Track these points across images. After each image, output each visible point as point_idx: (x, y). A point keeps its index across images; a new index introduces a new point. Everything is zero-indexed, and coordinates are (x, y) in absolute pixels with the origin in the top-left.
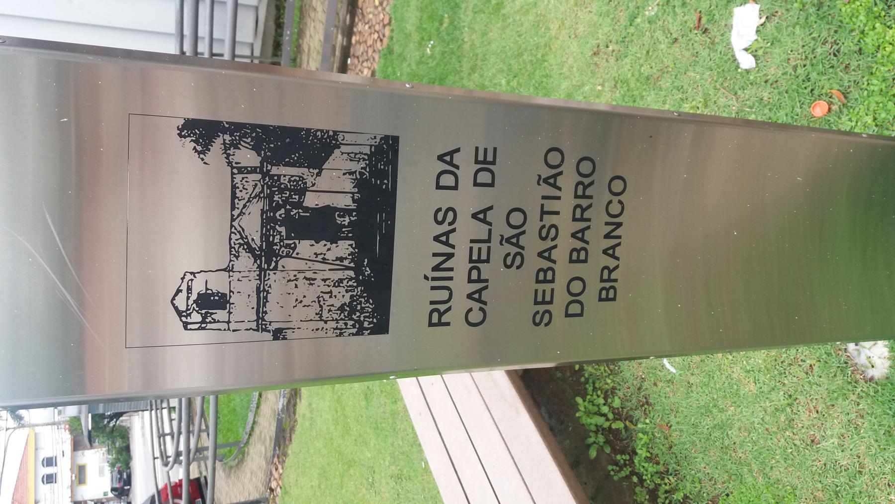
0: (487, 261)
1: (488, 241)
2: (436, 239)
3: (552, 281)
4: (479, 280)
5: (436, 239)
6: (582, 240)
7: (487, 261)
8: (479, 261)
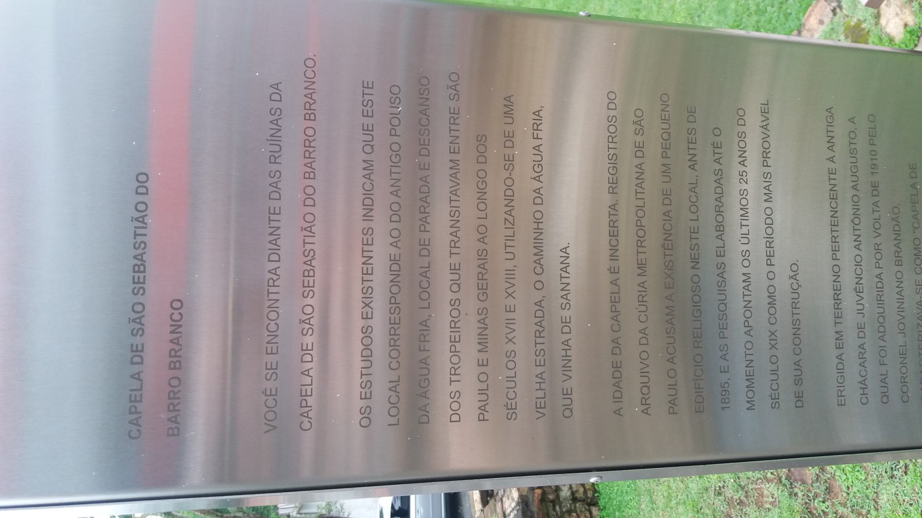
0: (141, 401)
1: (141, 389)
2: (135, 257)
3: (144, 272)
4: (136, 412)
5: (135, 257)
6: (141, 260)
7: (141, 401)
8: (136, 401)
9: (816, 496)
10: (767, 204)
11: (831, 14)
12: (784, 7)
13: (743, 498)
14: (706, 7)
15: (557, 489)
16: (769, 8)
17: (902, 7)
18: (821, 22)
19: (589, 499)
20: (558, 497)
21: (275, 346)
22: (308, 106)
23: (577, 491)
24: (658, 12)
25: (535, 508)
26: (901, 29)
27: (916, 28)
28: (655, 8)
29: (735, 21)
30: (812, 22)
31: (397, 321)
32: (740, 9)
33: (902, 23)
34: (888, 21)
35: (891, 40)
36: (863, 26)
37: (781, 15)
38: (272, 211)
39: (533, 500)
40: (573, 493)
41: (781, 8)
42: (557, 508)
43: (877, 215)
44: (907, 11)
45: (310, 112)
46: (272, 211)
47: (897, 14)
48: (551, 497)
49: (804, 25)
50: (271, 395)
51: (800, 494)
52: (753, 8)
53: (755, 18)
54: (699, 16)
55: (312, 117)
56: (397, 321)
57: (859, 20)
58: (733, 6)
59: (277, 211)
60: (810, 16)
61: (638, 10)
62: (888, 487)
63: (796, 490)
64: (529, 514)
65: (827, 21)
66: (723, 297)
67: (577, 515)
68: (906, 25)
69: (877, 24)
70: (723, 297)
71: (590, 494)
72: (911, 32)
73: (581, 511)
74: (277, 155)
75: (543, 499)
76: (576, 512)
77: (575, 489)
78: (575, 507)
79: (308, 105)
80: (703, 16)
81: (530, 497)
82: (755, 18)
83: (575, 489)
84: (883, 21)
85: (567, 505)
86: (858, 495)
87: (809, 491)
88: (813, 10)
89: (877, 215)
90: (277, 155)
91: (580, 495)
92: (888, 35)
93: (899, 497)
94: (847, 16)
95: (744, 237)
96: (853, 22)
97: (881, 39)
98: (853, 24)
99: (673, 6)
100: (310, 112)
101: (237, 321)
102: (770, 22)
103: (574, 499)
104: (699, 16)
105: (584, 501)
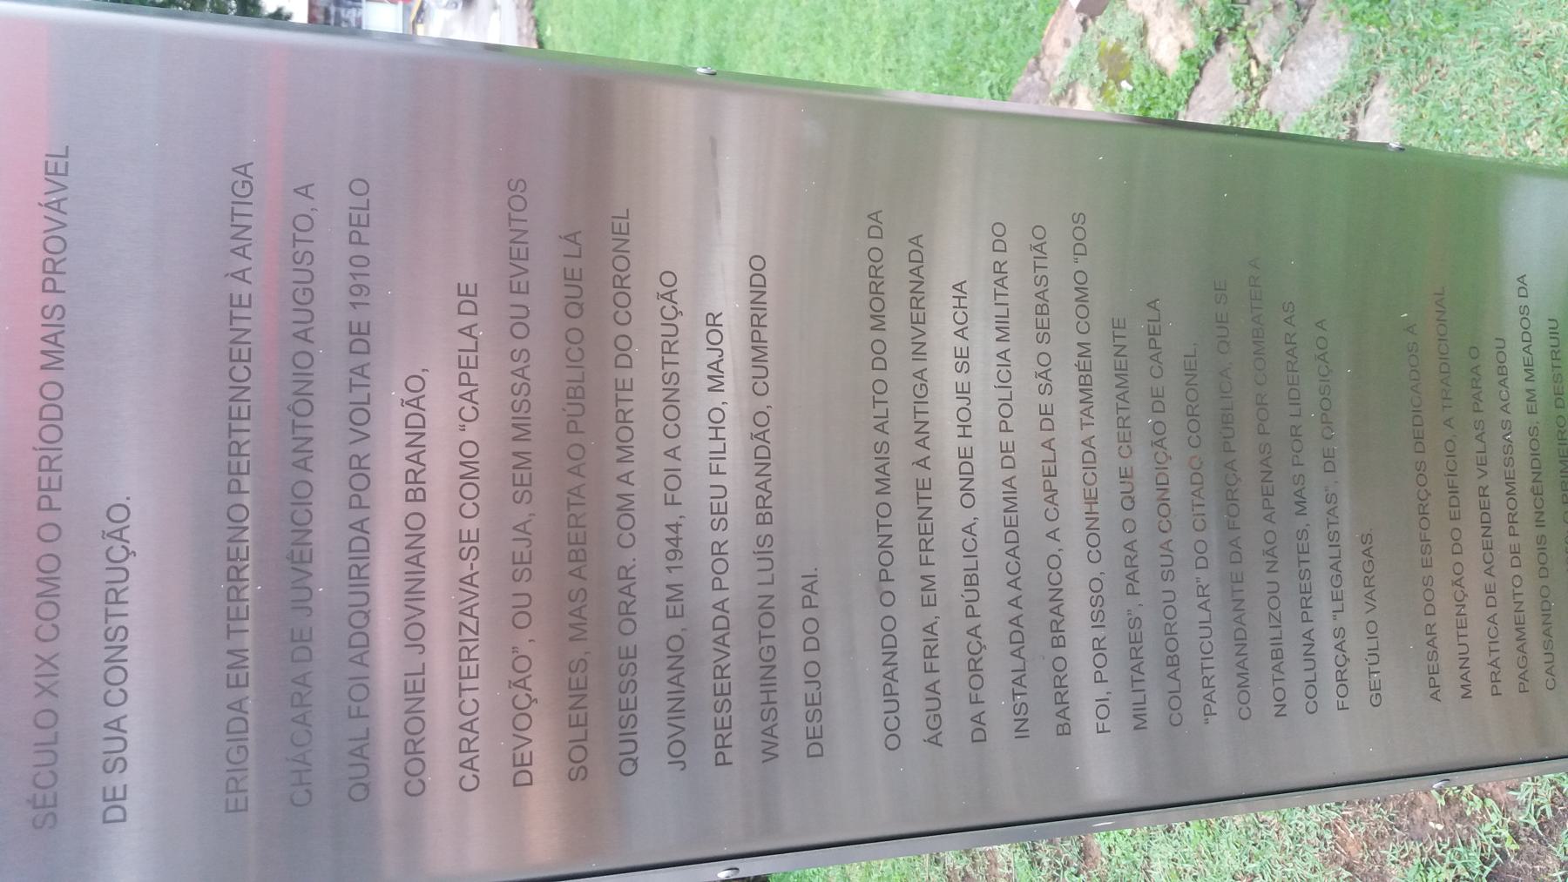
9: (1068, 864)
10: (876, 335)
11: (1080, 28)
12: (1024, 17)
13: (969, 869)
14: (916, 19)
16: (1002, 20)
17: (1177, 16)
18: (1067, 43)
21: (245, 348)
22: (411, 477)
24: (850, 27)
26: (1177, 53)
27: (1195, 52)
28: (845, 22)
29: (954, 42)
30: (1054, 44)
32: (963, 21)
33: (1177, 45)
34: (1159, 39)
35: (1162, 73)
36: (1124, 49)
37: (1019, 34)
38: (236, 302)
41: (1018, 19)
44: (1183, 23)
45: (415, 487)
46: (236, 302)
47: (1171, 29)
49: (1044, 48)
50: (240, 360)
51: (1045, 861)
52: (980, 20)
53: (983, 37)
54: (906, 35)
55: (420, 495)
57: (1118, 39)
58: (951, 16)
59: (245, 302)
60: (1052, 31)
61: (821, 24)
62: (1163, 848)
63: (1040, 854)
65: (1074, 41)
68: (1183, 48)
69: (1143, 45)
72: (1189, 60)
79: (411, 474)
80: (911, 34)
82: (983, 37)
84: (1151, 41)
86: (1123, 862)
87: (1058, 855)
88: (1055, 23)
92: (1158, 65)
93: (1179, 866)
94: (1103, 33)
96: (1110, 43)
97: (1148, 72)
98: (1110, 46)
99: (869, 17)
100: (415, 487)
102: (1003, 44)
104: (906, 35)
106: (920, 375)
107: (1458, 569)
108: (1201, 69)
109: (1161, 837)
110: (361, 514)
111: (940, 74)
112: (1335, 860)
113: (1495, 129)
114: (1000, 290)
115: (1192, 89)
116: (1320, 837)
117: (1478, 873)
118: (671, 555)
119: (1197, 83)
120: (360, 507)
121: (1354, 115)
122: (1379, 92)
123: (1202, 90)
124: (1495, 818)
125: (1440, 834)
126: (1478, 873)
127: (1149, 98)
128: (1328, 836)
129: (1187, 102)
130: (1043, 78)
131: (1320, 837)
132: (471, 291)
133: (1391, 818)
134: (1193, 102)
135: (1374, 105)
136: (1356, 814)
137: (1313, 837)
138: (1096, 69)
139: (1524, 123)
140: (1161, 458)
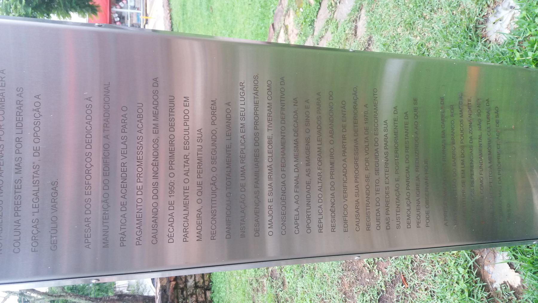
15: (186, 279)
19: (205, 286)
20: (186, 286)
23: (199, 282)
25: (169, 293)
31: (19, 203)
39: (169, 288)
40: (196, 283)
42: (185, 293)
43: (187, 168)
48: (181, 286)
56: (19, 203)
64: (165, 296)
66: (377, 160)
67: (197, 296)
70: (377, 160)
71: (206, 283)
73: (199, 294)
74: (172, 108)
75: (176, 287)
76: (196, 295)
77: (197, 281)
78: (196, 292)
81: (168, 287)
83: (197, 281)
85: (191, 291)
89: (187, 168)
90: (172, 108)
91: (200, 284)
95: (44, 291)
101: (376, 105)
103: (196, 286)
105: (203, 287)
106: (17, 222)
107: (397, 186)
108: (320, 4)
109: (300, 279)
110: (18, 218)
111: (261, 6)
112: (341, 291)
113: (389, 25)
114: (256, 96)
115: (318, 12)
116: (338, 282)
117: (376, 298)
118: (171, 192)
119: (319, 9)
120: (18, 216)
121: (356, 20)
122: (363, 11)
123: (320, 11)
124: (381, 278)
125: (368, 283)
126: (376, 298)
127: (307, 15)
128: (340, 282)
129: (317, 16)
130: (282, 7)
131: (338, 282)
132: (38, 149)
133: (356, 277)
134: (318, 16)
135: (361, 16)
136: (348, 274)
137: (336, 282)
138: (294, 4)
139: (397, 23)
140: (214, 189)
